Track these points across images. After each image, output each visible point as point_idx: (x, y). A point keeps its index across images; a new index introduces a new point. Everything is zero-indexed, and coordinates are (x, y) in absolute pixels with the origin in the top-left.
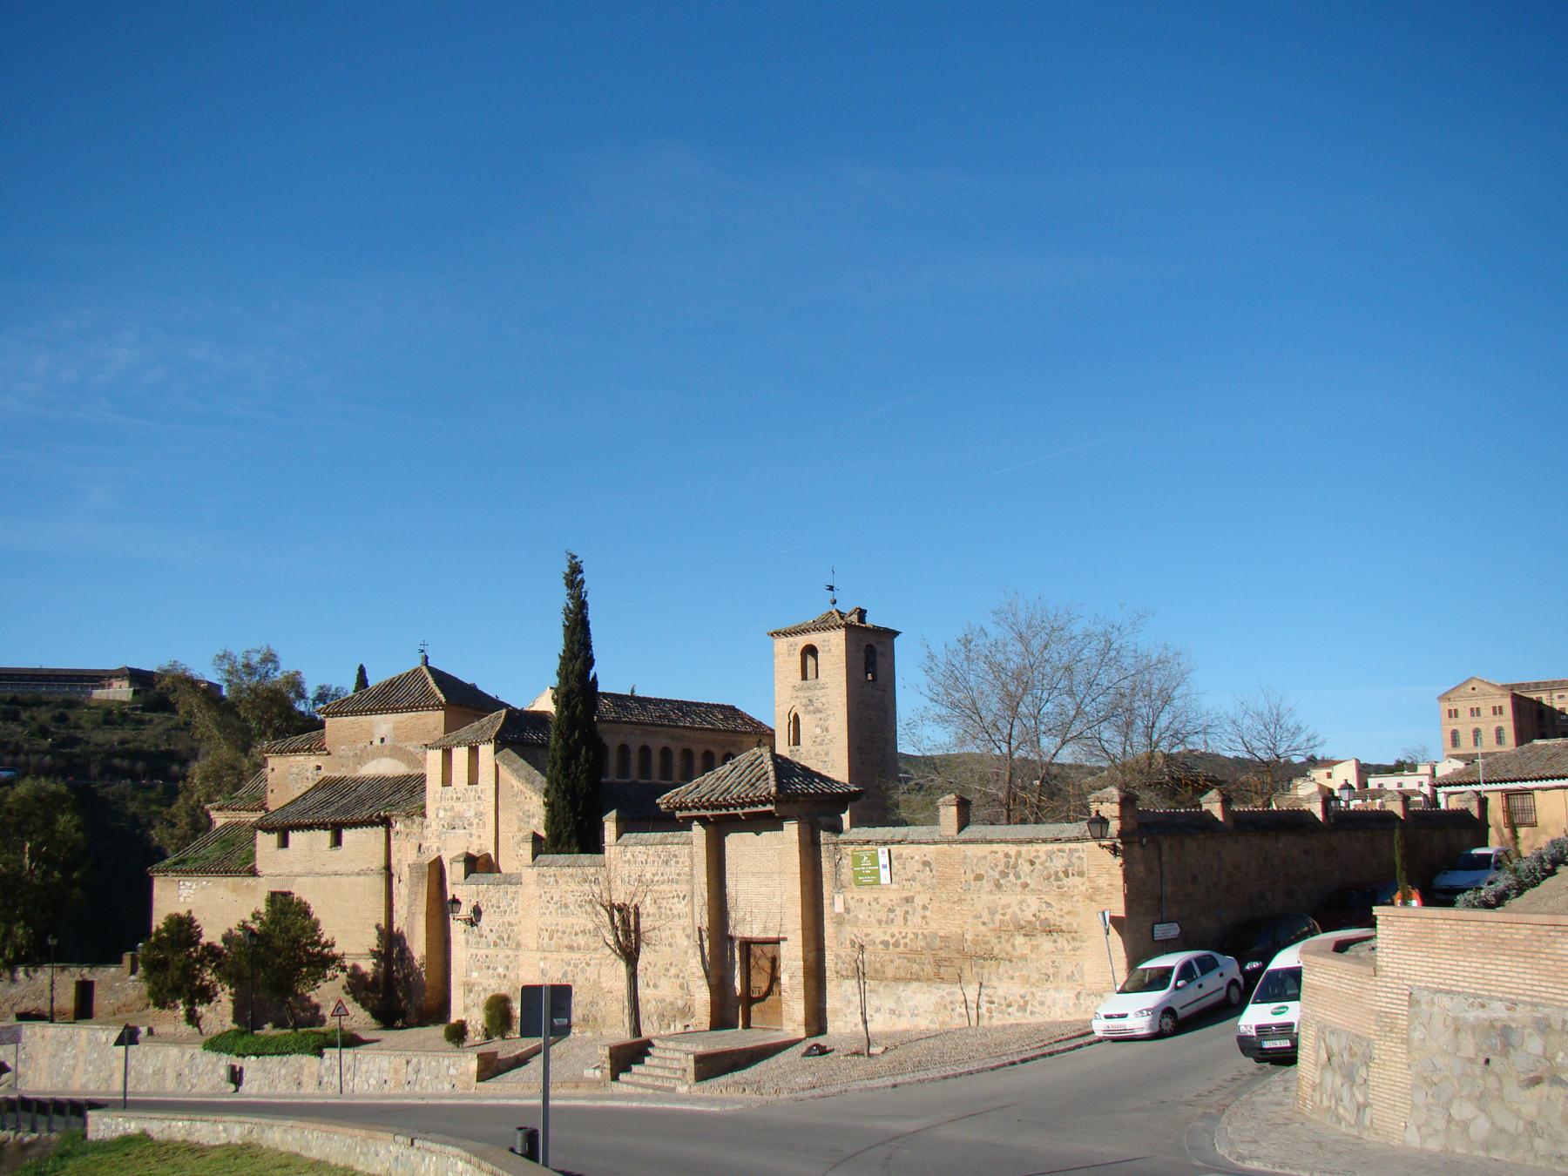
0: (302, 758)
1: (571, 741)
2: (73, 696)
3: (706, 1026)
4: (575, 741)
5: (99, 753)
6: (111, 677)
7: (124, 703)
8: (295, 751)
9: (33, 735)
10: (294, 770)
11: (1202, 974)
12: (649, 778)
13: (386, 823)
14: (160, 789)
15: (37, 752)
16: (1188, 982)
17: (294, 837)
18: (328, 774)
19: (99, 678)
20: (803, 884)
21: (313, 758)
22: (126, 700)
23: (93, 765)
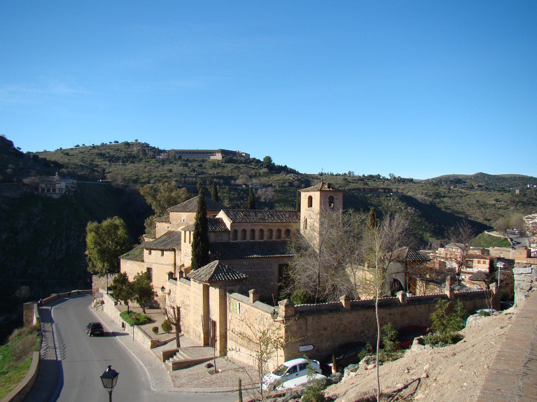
0: (164, 224)
1: (197, 240)
2: (205, 159)
3: (202, 345)
4: (198, 240)
5: (210, 177)
6: (216, 152)
7: (219, 160)
8: (162, 222)
9: (191, 171)
10: (162, 227)
11: (300, 370)
12: (254, 239)
13: (174, 250)
14: (227, 188)
15: (192, 177)
16: (290, 374)
17: (153, 251)
18: (170, 230)
19: (212, 153)
20: (220, 308)
21: (167, 224)
22: (220, 159)
23: (207, 181)
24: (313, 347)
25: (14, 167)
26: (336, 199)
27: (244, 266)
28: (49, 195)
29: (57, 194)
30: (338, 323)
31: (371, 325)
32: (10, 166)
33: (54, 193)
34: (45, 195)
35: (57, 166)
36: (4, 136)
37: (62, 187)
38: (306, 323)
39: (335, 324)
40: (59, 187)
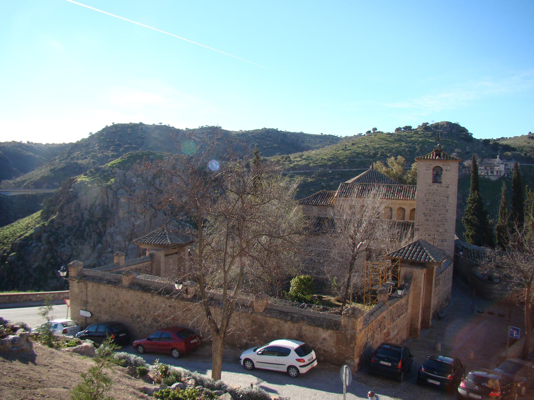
24: (90, 315)
25: (460, 151)
26: (446, 170)
27: (323, 244)
28: (486, 177)
29: (494, 176)
30: (116, 298)
31: (148, 312)
32: (457, 150)
33: (491, 176)
34: (483, 177)
35: (507, 148)
36: (458, 123)
37: (500, 170)
38: (87, 289)
39: (113, 298)
40: (497, 169)
